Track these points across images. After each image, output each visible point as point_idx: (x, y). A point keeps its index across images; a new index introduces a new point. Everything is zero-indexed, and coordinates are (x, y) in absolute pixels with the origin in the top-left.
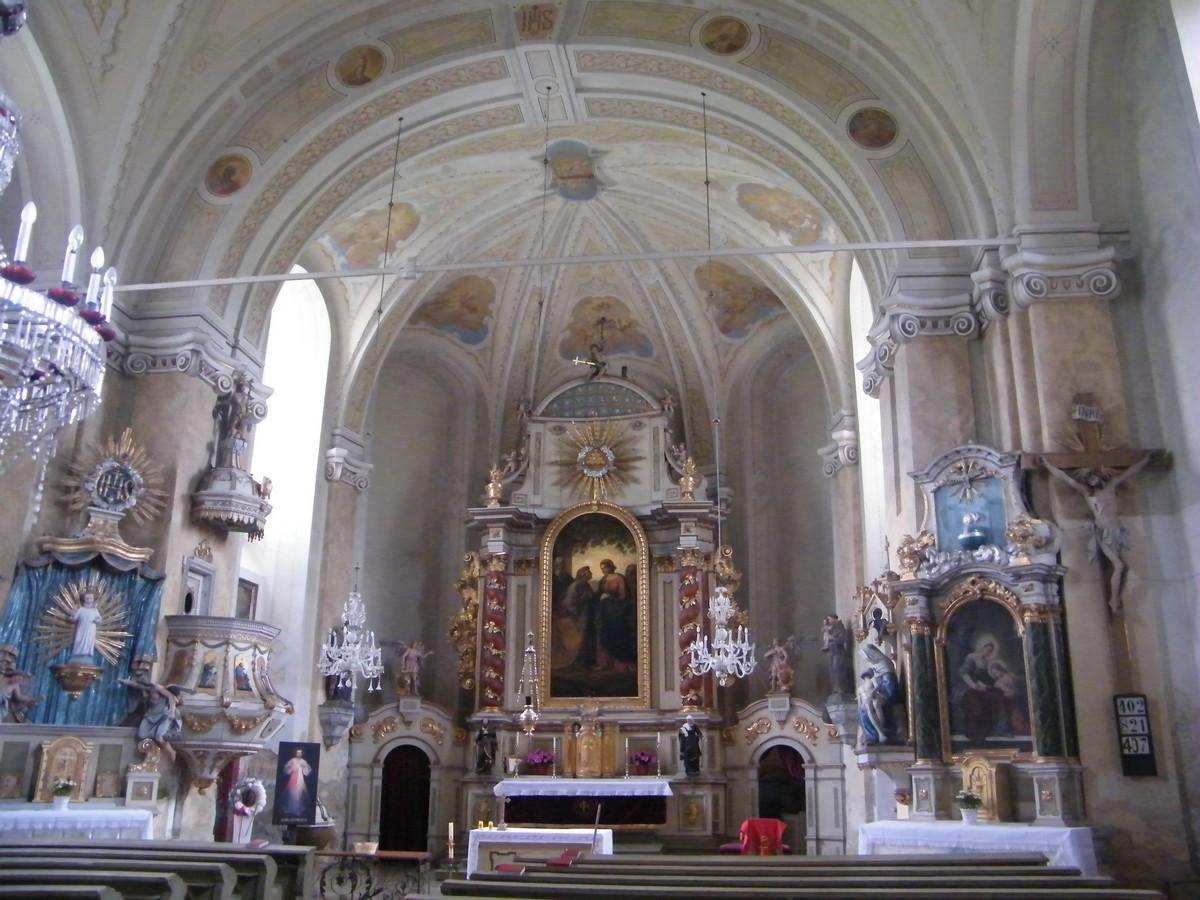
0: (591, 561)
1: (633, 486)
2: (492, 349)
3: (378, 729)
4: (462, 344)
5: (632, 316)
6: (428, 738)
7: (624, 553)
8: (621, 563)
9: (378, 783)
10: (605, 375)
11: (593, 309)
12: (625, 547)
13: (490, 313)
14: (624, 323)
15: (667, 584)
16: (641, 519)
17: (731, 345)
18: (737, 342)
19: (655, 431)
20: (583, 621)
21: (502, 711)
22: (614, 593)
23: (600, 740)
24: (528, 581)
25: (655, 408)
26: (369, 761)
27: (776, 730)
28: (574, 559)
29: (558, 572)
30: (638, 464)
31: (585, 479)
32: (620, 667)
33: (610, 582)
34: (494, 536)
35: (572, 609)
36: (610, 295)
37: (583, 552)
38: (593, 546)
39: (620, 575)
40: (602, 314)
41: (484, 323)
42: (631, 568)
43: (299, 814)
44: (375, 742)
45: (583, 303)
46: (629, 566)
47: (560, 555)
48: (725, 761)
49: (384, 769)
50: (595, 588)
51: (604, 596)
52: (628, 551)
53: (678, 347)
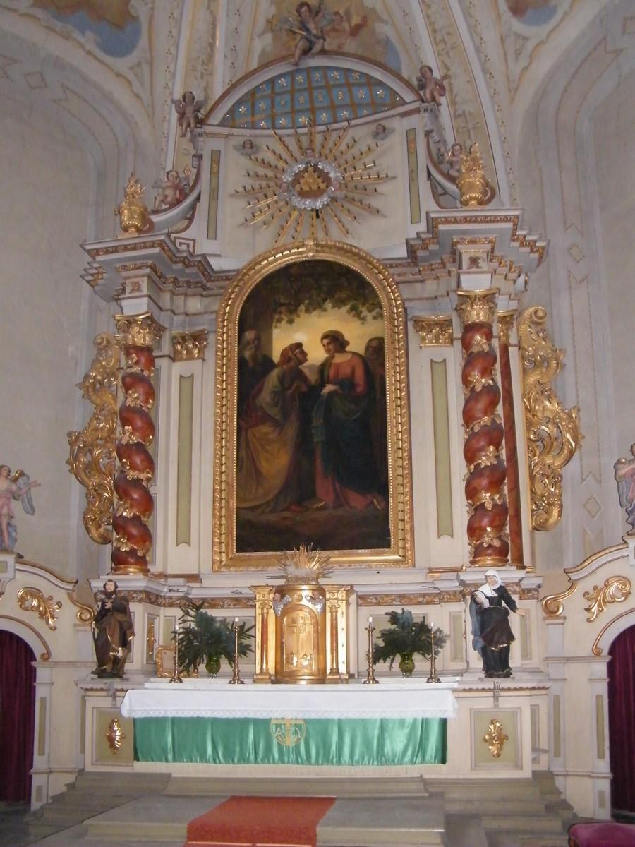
0: (305, 334)
1: (375, 222)
7: (363, 319)
8: (358, 335)
10: (323, 52)
12: (365, 313)
14: (356, 20)
16: (392, 264)
17: (525, 39)
18: (536, 32)
19: (411, 136)
20: (291, 430)
21: (146, 572)
22: (347, 384)
24: (193, 367)
25: (407, 100)
28: (276, 332)
29: (247, 354)
31: (295, 214)
32: (358, 502)
33: (338, 365)
34: (132, 291)
35: (273, 412)
37: (291, 322)
38: (307, 311)
39: (354, 353)
41: (133, 12)
42: (374, 344)
43: (337, 566)
46: (371, 340)
47: (251, 328)
48: (558, 775)
50: (313, 378)
51: (329, 388)
52: (369, 316)
53: (443, 40)
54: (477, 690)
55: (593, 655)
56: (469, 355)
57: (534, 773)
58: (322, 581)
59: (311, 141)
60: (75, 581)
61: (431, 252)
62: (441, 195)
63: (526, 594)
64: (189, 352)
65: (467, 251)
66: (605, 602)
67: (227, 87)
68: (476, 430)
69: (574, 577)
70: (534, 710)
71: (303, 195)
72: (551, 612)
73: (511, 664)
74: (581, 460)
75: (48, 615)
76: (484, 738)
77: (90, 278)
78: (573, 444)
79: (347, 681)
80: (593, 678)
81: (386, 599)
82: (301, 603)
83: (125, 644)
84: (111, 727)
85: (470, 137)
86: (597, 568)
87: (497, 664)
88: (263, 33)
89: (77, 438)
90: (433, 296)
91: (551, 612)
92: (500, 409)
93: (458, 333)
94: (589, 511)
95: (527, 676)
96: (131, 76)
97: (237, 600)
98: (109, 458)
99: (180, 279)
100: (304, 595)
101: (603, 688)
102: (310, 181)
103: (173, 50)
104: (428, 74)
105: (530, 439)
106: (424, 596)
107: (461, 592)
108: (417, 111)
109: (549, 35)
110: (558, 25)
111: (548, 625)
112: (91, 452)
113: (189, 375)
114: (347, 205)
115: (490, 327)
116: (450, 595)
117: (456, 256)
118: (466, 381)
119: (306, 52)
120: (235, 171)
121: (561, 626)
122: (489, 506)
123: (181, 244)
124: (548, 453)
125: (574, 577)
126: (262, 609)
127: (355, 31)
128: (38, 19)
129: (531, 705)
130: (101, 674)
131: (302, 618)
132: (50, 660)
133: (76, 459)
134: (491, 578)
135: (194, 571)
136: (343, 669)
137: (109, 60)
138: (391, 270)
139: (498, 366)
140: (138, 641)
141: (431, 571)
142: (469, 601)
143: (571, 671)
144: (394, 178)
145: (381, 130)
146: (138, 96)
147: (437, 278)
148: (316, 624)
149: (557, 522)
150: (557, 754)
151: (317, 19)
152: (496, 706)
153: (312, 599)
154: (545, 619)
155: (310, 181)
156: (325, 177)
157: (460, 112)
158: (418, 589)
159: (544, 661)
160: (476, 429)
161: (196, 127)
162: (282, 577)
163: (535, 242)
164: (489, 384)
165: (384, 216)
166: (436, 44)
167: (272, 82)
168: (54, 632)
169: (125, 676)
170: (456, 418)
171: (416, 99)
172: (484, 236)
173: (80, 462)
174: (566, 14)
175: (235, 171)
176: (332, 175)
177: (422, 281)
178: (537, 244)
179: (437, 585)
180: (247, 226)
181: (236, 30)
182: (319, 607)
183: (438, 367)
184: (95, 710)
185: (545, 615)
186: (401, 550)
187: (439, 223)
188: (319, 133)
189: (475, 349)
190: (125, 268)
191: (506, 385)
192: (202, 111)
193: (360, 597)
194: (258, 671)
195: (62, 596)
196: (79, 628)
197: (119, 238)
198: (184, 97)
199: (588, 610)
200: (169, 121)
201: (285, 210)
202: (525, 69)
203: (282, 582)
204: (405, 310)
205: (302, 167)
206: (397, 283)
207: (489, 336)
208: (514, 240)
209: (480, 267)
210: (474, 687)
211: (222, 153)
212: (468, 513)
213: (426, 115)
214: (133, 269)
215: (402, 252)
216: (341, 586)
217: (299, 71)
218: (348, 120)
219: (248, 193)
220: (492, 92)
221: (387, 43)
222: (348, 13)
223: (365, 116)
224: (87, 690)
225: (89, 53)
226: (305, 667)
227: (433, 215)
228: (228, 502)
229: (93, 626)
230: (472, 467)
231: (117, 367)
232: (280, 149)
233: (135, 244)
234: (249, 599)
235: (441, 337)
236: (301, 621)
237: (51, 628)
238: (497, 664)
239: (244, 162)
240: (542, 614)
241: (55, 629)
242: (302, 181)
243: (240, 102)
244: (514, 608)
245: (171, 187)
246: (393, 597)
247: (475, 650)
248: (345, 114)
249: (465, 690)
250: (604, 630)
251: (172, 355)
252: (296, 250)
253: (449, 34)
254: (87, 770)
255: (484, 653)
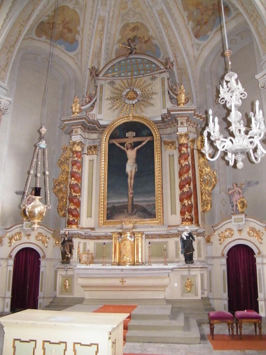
1: (151, 108)
2: (81, 54)
3: (11, 239)
4: (66, 51)
5: (150, 34)
6: (40, 243)
9: (11, 268)
10: (136, 53)
11: (130, 30)
13: (78, 32)
14: (146, 39)
15: (171, 156)
16: (156, 122)
17: (200, 45)
18: (203, 43)
19: (163, 79)
21: (78, 227)
23: (133, 243)
24: (95, 157)
25: (162, 68)
26: (6, 256)
27: (236, 235)
30: (154, 96)
31: (126, 105)
36: (138, 20)
40: (135, 33)
41: (76, 39)
44: (10, 246)
45: (126, 26)
48: (211, 299)
49: (14, 261)
53: (174, 46)
54: (183, 268)
55: (221, 256)
56: (180, 154)
57: (202, 298)
58: (134, 230)
59: (132, 82)
60: (54, 230)
61: (169, 120)
62: (173, 99)
63: (199, 235)
64: (93, 152)
65: (180, 120)
66: (225, 237)
67: (104, 65)
68: (183, 179)
69: (215, 228)
70: (202, 276)
71: (129, 99)
72: (208, 241)
73: (194, 259)
74: (220, 186)
75: (45, 242)
76: (185, 285)
77: (61, 128)
78: (215, 182)
79: (141, 265)
80: (222, 264)
81: (154, 236)
82: (127, 238)
83: (71, 252)
84: (65, 281)
85: (183, 76)
86: (223, 226)
87: (189, 259)
88: (117, 43)
89: (56, 181)
90: (169, 133)
91: (208, 241)
92: (190, 172)
93: (177, 146)
94: (223, 204)
95: (199, 263)
96: (75, 58)
97: (106, 236)
98: (66, 188)
99: (90, 128)
100: (128, 235)
101: (225, 268)
102: (131, 95)
103: (88, 50)
104: (168, 60)
105: (201, 181)
106: (167, 235)
107: (178, 234)
108: (165, 72)
109: (207, 44)
110: (209, 41)
111: (207, 245)
112: (60, 185)
113: (92, 160)
114: (143, 103)
115: (187, 144)
116: (175, 235)
117: (177, 121)
118: (180, 163)
119: (130, 53)
120: (107, 91)
121: (211, 246)
122: (187, 204)
123: (90, 116)
124: (207, 185)
125: (215, 228)
126: (115, 240)
127: (146, 42)
128: (47, 42)
129: (201, 274)
130: (63, 263)
131: (127, 243)
132: (45, 258)
133: (55, 188)
134: (187, 229)
135: (93, 227)
136: (140, 261)
137: (69, 53)
138: (156, 124)
139: (190, 157)
140: (75, 252)
141: (169, 226)
142: (180, 237)
143: (215, 261)
144: (157, 93)
145: (154, 77)
146: (77, 64)
147: (171, 127)
148: (131, 245)
149: (210, 210)
150: (211, 291)
151: (134, 43)
152: (189, 274)
153: (131, 237)
154: (206, 243)
155: (131, 95)
156: (136, 93)
157: (179, 68)
158: (165, 232)
159: (206, 258)
160: (183, 179)
161: (96, 77)
162: (121, 229)
163: (202, 116)
164: (187, 164)
165: (154, 106)
166: (171, 47)
167: (119, 62)
168: (47, 248)
169: (70, 263)
170: (177, 175)
171: (164, 68)
172: (185, 115)
173: (56, 189)
174: (212, 38)
175: (107, 91)
176: (138, 93)
177: (166, 128)
178: (202, 116)
179: (171, 231)
180: (111, 109)
181: (108, 43)
182: (133, 239)
183: (171, 156)
184: (60, 275)
185: (206, 242)
186: (159, 219)
187: (171, 111)
188: (134, 78)
189: (182, 152)
190: (73, 125)
191: (193, 163)
192: (97, 72)
193: (146, 235)
194: (113, 261)
195: (50, 235)
196: (55, 247)
197: (72, 116)
198: (92, 68)
199: (220, 240)
200: (87, 72)
201: (123, 104)
202: (200, 54)
203: (121, 231)
204: (161, 138)
205: (129, 90)
206: (158, 129)
207: (187, 148)
208: (195, 116)
209: (184, 125)
210: (182, 267)
211: (104, 85)
212: (180, 207)
213: (168, 73)
214: (76, 126)
215: (160, 119)
216: (139, 232)
217: (128, 59)
218: (143, 74)
219: (112, 98)
220: (190, 62)
221: (156, 46)
222: (144, 37)
223: (148, 73)
224: (58, 268)
225: (62, 51)
226: (128, 260)
227: (169, 109)
228: (104, 202)
229: (61, 246)
230: (181, 191)
231: (69, 156)
232: (122, 84)
233: (77, 118)
234: (110, 236)
235: (172, 147)
236: (127, 244)
237: (46, 247)
238: (189, 259)
239: (110, 87)
240: (205, 242)
241: (47, 247)
242: (128, 95)
243: (109, 69)
244: (194, 240)
245: (88, 97)
246: (157, 235)
247: (182, 254)
248: (142, 72)
249: (179, 268)
250: (225, 247)
251: (87, 153)
252: (126, 118)
253: (175, 44)
254: (57, 296)
255: (185, 255)
